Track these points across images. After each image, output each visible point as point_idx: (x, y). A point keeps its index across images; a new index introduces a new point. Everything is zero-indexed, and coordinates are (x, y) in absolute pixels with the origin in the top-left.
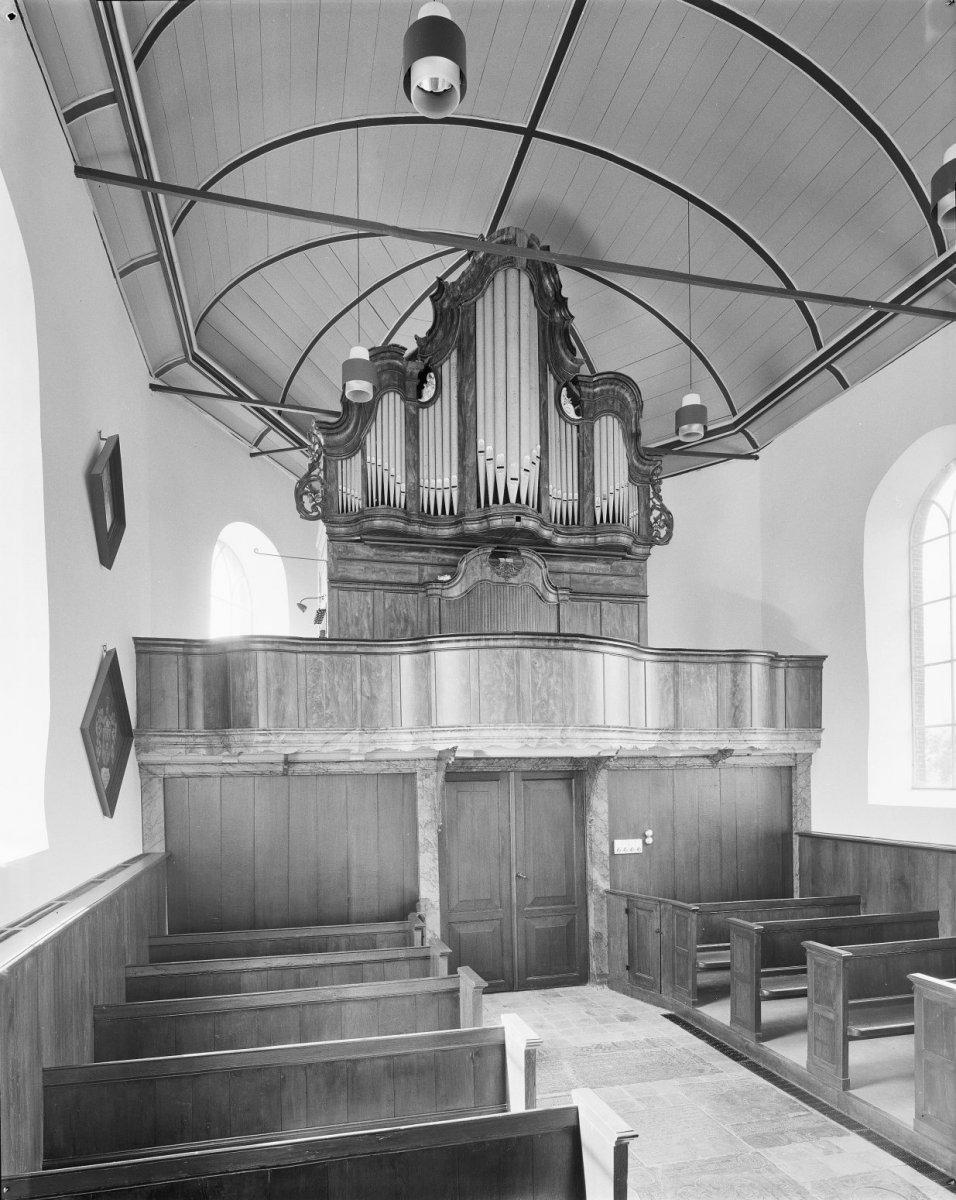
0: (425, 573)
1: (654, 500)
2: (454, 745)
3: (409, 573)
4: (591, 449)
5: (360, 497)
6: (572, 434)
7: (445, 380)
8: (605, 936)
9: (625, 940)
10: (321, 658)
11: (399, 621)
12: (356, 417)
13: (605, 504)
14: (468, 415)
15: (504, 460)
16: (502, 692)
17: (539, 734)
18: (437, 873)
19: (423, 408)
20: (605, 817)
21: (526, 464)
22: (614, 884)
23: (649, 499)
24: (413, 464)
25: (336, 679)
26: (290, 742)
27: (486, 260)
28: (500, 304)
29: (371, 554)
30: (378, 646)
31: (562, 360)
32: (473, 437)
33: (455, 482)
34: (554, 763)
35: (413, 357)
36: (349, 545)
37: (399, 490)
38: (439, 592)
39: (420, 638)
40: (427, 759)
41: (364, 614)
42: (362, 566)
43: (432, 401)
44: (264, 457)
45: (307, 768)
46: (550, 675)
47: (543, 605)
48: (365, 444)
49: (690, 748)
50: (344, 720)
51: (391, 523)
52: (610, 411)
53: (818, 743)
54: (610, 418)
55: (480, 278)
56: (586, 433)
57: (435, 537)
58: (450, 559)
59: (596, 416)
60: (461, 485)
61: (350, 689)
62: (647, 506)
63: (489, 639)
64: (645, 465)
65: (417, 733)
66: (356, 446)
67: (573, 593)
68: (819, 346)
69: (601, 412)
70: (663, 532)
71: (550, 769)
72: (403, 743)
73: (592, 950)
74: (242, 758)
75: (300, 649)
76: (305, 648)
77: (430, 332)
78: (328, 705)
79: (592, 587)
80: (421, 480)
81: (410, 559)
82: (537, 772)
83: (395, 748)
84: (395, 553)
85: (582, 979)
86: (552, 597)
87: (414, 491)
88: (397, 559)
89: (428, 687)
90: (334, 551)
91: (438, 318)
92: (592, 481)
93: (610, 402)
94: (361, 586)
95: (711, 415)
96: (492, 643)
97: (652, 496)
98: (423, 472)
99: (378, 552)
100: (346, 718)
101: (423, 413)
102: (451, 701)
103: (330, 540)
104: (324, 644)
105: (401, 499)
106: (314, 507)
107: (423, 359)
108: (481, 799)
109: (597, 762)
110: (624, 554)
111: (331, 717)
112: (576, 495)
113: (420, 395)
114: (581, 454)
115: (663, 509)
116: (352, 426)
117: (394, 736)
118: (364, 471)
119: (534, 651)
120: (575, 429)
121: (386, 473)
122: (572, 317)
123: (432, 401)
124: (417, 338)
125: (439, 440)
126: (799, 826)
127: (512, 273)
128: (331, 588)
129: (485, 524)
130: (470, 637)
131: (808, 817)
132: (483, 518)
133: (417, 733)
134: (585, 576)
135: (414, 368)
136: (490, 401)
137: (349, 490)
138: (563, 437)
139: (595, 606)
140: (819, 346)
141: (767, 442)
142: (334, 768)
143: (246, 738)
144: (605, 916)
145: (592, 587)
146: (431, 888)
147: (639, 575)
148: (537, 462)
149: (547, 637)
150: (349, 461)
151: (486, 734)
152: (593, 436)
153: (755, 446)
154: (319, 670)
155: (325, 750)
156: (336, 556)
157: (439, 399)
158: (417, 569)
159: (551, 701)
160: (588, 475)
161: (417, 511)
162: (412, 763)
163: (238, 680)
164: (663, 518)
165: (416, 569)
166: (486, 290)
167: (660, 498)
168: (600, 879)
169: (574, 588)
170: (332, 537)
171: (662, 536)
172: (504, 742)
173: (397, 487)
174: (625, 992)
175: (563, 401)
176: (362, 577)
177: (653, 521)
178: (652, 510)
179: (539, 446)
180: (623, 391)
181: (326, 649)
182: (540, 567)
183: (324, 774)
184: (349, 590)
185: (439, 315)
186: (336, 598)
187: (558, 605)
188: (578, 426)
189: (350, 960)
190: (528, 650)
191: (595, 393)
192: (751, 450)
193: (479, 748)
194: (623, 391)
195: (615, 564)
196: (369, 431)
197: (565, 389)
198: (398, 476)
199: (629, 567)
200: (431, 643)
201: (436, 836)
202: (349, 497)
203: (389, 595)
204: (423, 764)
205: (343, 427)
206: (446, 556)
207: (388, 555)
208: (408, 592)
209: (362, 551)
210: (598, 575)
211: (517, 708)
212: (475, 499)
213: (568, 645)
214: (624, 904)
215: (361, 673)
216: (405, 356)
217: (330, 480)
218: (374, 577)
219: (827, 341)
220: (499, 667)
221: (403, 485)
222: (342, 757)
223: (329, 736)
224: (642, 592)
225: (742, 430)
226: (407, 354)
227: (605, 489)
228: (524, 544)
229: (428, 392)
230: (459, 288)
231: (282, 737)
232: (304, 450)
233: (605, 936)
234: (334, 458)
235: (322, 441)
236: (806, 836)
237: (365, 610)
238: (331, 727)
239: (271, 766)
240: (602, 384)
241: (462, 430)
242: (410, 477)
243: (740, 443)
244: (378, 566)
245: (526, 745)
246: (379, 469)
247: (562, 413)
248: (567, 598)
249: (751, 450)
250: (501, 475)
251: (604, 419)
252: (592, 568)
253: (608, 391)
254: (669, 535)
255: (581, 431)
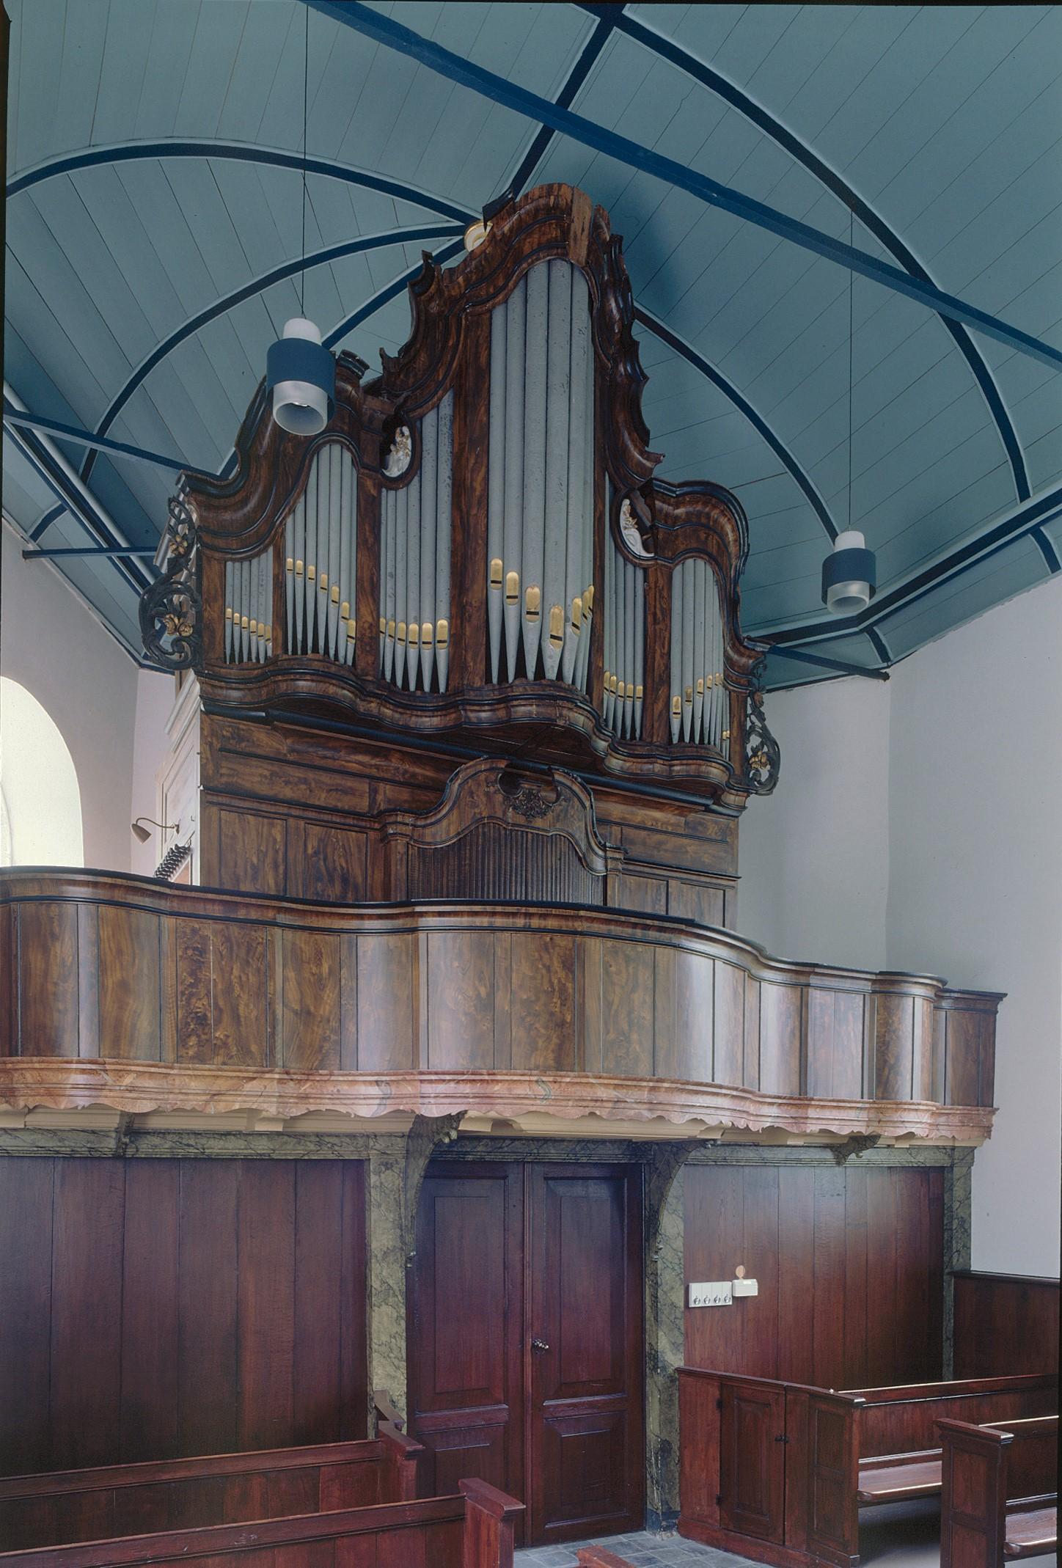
0: (380, 798)
1: (753, 717)
2: (462, 1108)
3: (350, 792)
4: (667, 613)
5: (269, 635)
6: (635, 581)
7: (429, 445)
8: (675, 1447)
9: (714, 1452)
10: (208, 929)
11: (331, 880)
12: (268, 470)
13: (688, 708)
14: (474, 512)
15: (538, 601)
16: (552, 1014)
17: (613, 1094)
18: (403, 1345)
19: (389, 489)
20: (679, 1244)
21: (575, 616)
22: (688, 1360)
23: (747, 716)
24: (368, 588)
25: (236, 972)
26: (143, 1090)
27: (531, 227)
28: (537, 318)
29: (284, 749)
30: (318, 914)
31: (625, 448)
32: (480, 549)
33: (444, 634)
34: (601, 1150)
35: (374, 389)
36: (243, 725)
37: (342, 634)
38: (408, 830)
39: (401, 902)
40: (390, 1135)
41: (269, 860)
42: (264, 769)
43: (404, 479)
44: (44, 561)
45: (163, 1147)
46: (633, 991)
47: (583, 873)
48: (283, 535)
49: (821, 1131)
50: (249, 1052)
51: (332, 690)
52: (700, 551)
53: (987, 1131)
54: (701, 563)
55: (501, 268)
56: (661, 583)
57: (406, 730)
58: (425, 777)
59: (678, 558)
60: (456, 638)
61: (261, 993)
62: (742, 726)
63: (531, 915)
64: (742, 655)
65: (388, 1083)
66: (268, 538)
67: (629, 860)
68: (1024, 494)
69: (687, 551)
70: (765, 774)
71: (595, 1159)
72: (363, 1099)
73: (653, 1470)
74: (33, 1120)
75: (164, 905)
76: (175, 906)
77: (406, 350)
78: (218, 1021)
79: (655, 853)
80: (382, 620)
81: (354, 767)
82: (561, 1162)
83: (343, 1109)
84: (329, 753)
85: (636, 1520)
86: (599, 864)
87: (369, 639)
88: (329, 763)
89: (414, 997)
90: (213, 733)
91: (422, 329)
92: (668, 667)
93: (703, 536)
94: (264, 807)
95: (881, 569)
96: (535, 923)
97: (749, 711)
98: (386, 606)
99: (297, 747)
100: (254, 1048)
101: (388, 498)
102: (416, 1038)
103: (207, 713)
104: (213, 901)
105: (346, 650)
106: (176, 643)
107: (393, 396)
108: (478, 1215)
109: (678, 1150)
110: (709, 802)
111: (225, 1044)
112: (640, 688)
113: (384, 464)
114: (650, 619)
115: (766, 737)
116: (253, 502)
117: (345, 1088)
118: (279, 585)
119: (610, 943)
120: (640, 573)
121: (322, 594)
122: (646, 378)
123: (404, 479)
124: (383, 354)
125: (413, 554)
126: (957, 1263)
127: (561, 269)
128: (205, 804)
129: (502, 714)
130: (499, 909)
131: (967, 1247)
132: (499, 701)
133: (388, 1083)
134: (643, 833)
135: (377, 407)
136: (514, 492)
137: (245, 619)
138: (628, 588)
139: (659, 887)
140: (1024, 494)
141: (908, 648)
142: (216, 1147)
143: (52, 1077)
144: (675, 1411)
145: (655, 853)
146: (391, 1370)
147: (727, 839)
148: (590, 616)
149: (633, 920)
150: (246, 564)
151: (521, 1090)
152: (670, 589)
153: (884, 656)
154: (202, 952)
155: (211, 1109)
156: (217, 745)
157: (416, 479)
158: (366, 788)
159: (635, 1037)
160: (662, 657)
161: (367, 673)
162: (361, 1141)
163: (36, 959)
164: (765, 749)
165: (364, 786)
166: (512, 291)
167: (761, 717)
168: (670, 1351)
169: (636, 851)
170: (212, 707)
171: (763, 780)
172: (542, 1106)
173: (342, 623)
174: (712, 1542)
175: (622, 523)
176: (264, 790)
177: (750, 754)
178: (750, 734)
179: (592, 588)
180: (723, 520)
181: (217, 910)
182: (584, 807)
183: (192, 1164)
184: (241, 812)
185: (423, 323)
186: (215, 825)
187: (605, 878)
188: (645, 570)
189: (307, 1534)
190: (598, 940)
191: (677, 518)
192: (878, 664)
193: (507, 1113)
194: (723, 520)
195: (692, 816)
196: (292, 511)
197: (627, 502)
198: (345, 604)
199: (711, 824)
200: (422, 914)
201: (401, 1274)
202: (245, 633)
203: (316, 831)
204: (381, 1144)
205: (238, 498)
206: (418, 770)
207: (316, 754)
208: (348, 828)
209: (265, 740)
210: (665, 832)
211: (565, 1045)
212: (483, 667)
213: (665, 936)
214: (714, 1392)
215: (284, 966)
216: (362, 382)
217: (209, 596)
218: (288, 793)
219: (1039, 488)
220: (548, 969)
221: (353, 623)
222: (240, 1125)
223: (220, 1082)
224: (731, 872)
225: (869, 630)
226: (368, 377)
227: (688, 681)
228: (564, 764)
229: (399, 462)
230: (461, 279)
231: (128, 1080)
232: (114, 556)
233: (675, 1447)
234: (217, 555)
235: (195, 517)
236: (966, 1276)
237: (270, 853)
238: (224, 1064)
239: (92, 1137)
240: (690, 503)
241: (459, 538)
242: (364, 611)
243: (860, 649)
244: (297, 773)
245: (592, 1114)
246: (310, 584)
247: (621, 545)
248: (620, 866)
249: (878, 664)
250: (532, 626)
251: (690, 562)
252: (657, 820)
253: (699, 514)
254: (773, 778)
255: (652, 579)
